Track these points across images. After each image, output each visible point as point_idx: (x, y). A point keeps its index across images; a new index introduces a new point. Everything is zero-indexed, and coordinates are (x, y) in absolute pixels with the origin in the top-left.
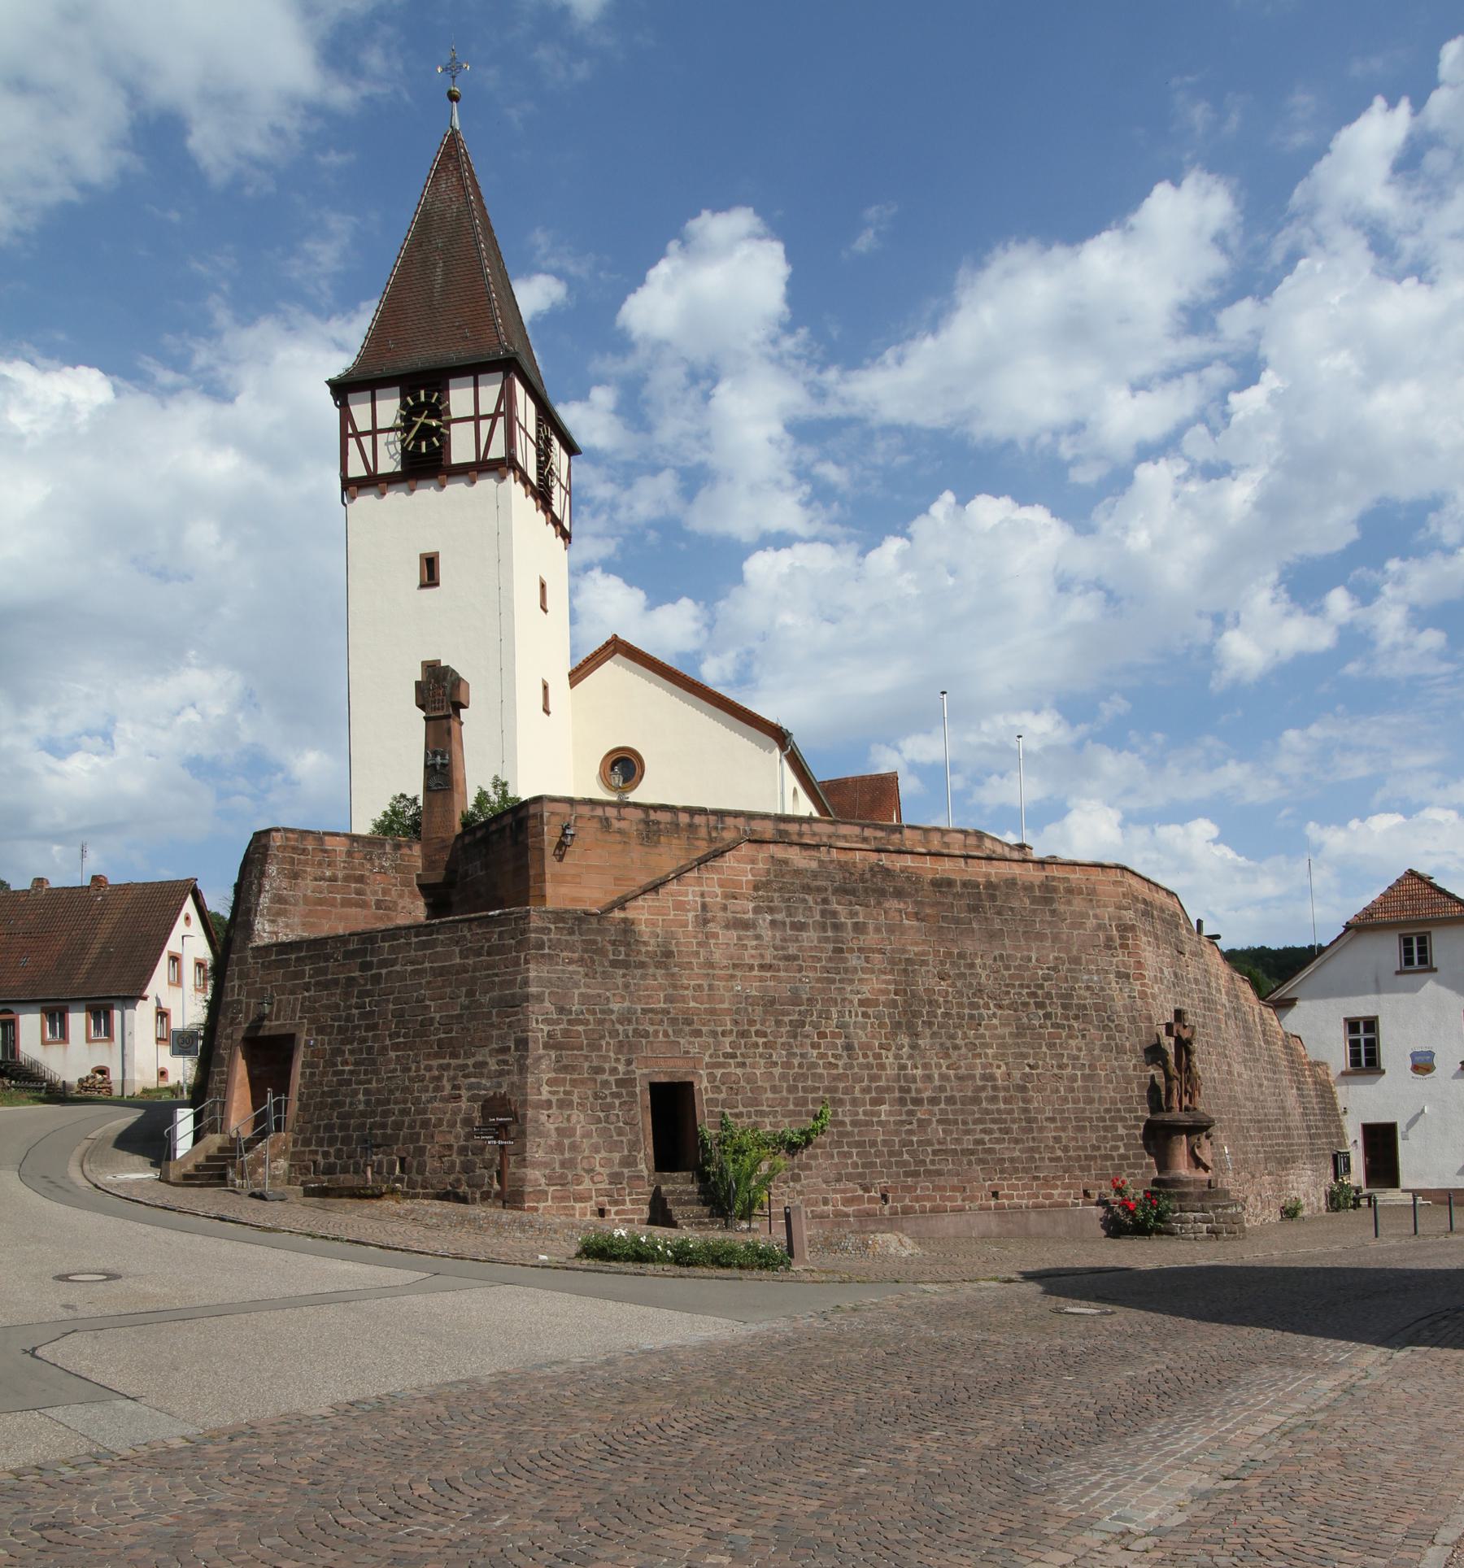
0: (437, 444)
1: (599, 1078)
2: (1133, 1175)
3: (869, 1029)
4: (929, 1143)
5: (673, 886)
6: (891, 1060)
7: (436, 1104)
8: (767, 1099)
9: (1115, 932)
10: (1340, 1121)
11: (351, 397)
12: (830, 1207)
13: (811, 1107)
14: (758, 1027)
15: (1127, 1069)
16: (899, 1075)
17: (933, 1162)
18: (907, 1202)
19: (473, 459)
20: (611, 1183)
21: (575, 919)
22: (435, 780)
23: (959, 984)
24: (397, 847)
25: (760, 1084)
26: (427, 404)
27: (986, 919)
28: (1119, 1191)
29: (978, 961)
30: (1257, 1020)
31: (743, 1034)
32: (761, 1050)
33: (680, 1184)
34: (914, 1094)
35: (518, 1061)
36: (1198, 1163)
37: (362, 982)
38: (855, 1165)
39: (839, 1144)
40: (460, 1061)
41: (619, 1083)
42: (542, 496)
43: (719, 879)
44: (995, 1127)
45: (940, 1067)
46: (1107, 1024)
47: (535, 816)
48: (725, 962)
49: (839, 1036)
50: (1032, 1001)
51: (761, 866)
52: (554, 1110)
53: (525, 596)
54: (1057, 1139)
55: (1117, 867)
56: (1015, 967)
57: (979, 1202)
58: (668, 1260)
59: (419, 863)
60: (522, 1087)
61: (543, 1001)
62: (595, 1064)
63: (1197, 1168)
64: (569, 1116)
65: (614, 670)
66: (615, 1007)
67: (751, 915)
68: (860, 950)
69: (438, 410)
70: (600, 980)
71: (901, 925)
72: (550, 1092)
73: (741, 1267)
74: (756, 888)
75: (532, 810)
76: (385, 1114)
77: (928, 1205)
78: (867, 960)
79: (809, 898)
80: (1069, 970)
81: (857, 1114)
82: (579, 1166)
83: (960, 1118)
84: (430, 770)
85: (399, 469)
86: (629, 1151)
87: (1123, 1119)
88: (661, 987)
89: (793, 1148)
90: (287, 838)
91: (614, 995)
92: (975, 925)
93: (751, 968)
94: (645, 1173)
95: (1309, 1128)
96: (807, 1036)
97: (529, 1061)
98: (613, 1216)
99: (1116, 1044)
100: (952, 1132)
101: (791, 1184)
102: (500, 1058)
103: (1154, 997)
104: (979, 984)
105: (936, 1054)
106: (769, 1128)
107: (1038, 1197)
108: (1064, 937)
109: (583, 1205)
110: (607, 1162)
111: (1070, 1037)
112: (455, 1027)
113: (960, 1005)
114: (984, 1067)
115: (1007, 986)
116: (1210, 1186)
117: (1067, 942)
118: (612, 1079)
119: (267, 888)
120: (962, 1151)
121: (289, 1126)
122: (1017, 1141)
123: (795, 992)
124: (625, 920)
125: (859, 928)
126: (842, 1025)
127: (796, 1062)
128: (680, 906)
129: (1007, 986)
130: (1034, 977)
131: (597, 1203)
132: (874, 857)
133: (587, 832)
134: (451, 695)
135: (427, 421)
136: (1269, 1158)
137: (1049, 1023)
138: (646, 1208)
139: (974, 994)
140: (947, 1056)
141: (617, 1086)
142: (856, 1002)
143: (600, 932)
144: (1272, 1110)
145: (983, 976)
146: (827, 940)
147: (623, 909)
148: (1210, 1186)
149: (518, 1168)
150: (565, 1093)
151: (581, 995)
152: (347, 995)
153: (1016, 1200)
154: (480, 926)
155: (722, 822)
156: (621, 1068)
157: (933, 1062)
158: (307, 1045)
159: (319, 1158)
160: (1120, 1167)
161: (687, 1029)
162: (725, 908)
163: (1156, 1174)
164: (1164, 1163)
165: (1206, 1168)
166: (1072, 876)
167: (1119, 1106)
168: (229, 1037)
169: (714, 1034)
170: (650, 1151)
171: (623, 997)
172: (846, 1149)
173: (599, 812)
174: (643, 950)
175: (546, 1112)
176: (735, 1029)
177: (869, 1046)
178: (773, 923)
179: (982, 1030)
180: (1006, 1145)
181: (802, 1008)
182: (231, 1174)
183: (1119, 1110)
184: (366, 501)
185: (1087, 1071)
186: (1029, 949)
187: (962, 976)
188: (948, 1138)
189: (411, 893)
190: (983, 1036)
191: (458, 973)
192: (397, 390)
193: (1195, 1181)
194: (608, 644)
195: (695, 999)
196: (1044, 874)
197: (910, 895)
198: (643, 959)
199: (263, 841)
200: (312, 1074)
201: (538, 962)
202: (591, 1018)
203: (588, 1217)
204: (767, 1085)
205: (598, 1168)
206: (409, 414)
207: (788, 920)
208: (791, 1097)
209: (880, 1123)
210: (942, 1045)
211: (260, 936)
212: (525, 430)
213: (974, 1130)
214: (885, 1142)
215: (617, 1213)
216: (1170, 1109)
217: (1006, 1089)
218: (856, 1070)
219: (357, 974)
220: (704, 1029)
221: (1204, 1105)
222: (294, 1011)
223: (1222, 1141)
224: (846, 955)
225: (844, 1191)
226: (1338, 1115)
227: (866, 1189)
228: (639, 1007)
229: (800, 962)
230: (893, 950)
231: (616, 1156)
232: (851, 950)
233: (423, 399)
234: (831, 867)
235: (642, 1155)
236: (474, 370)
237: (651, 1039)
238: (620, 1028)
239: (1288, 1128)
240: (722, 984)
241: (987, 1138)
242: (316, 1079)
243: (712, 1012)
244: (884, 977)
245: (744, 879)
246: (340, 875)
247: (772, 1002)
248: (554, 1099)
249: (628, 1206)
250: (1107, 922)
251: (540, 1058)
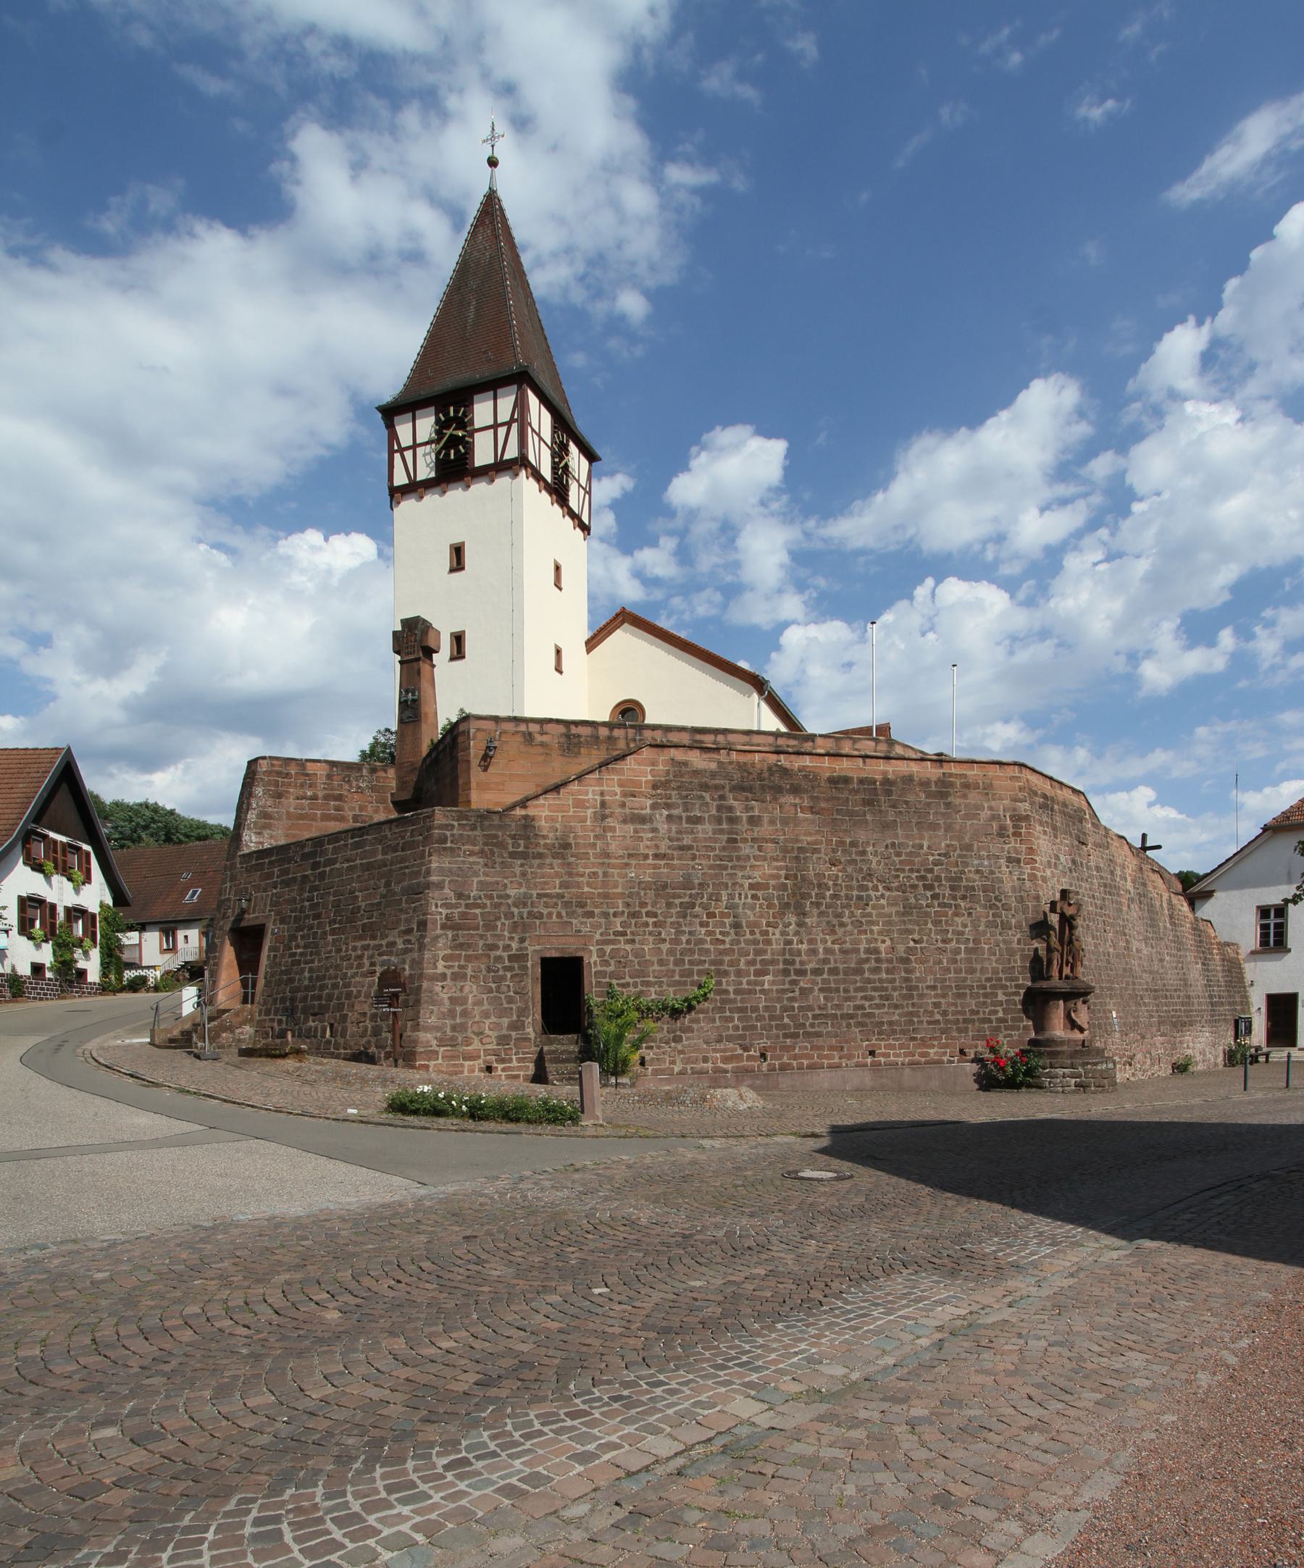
0: (463, 451)
1: (493, 954)
2: (1011, 1036)
3: (758, 910)
4: (810, 1008)
5: (574, 787)
6: (778, 936)
7: (357, 979)
8: (654, 971)
9: (1008, 822)
10: (1246, 992)
11: (397, 419)
12: (710, 1065)
13: (696, 978)
14: (649, 908)
15: (1011, 943)
16: (784, 949)
17: (812, 1025)
18: (785, 1059)
19: (492, 461)
20: (498, 1044)
21: (478, 816)
22: (408, 713)
23: (849, 869)
24: (373, 770)
25: (647, 958)
26: (456, 418)
27: (880, 811)
28: (993, 1050)
29: (870, 849)
30: (1165, 905)
31: (634, 915)
32: (651, 928)
33: (567, 1044)
34: (798, 966)
35: (418, 940)
36: (1073, 1025)
37: (312, 878)
38: (737, 1028)
39: (721, 1010)
40: (376, 942)
41: (511, 958)
42: (558, 491)
43: (619, 780)
44: (876, 994)
45: (824, 941)
46: (994, 899)
47: (463, 732)
48: (621, 852)
49: (728, 915)
50: (921, 883)
51: (661, 767)
52: (448, 982)
53: (536, 575)
54: (937, 1005)
55: (1015, 764)
56: (906, 853)
57: (856, 1060)
58: (463, 1115)
59: (394, 784)
60: (417, 964)
61: (442, 888)
62: (490, 942)
63: (1072, 1029)
64: (462, 987)
65: (623, 638)
66: (512, 892)
67: (648, 811)
68: (753, 840)
69: (464, 422)
70: (498, 869)
71: (796, 817)
72: (445, 967)
73: (529, 1121)
74: (655, 787)
75: (462, 727)
76: (322, 988)
77: (805, 1062)
78: (760, 849)
79: (707, 796)
80: (960, 856)
81: (741, 983)
82: (470, 1030)
83: (842, 987)
84: (403, 705)
85: (433, 475)
86: (518, 1017)
87: (1004, 987)
88: (557, 875)
89: (676, 1013)
90: (273, 765)
91: (511, 882)
92: (868, 817)
93: (646, 857)
94: (532, 1036)
95: (1211, 997)
96: (696, 916)
97: (427, 940)
98: (499, 1072)
99: (1002, 921)
100: (833, 999)
101: (673, 1044)
102: (406, 938)
103: (1044, 879)
104: (869, 869)
105: (822, 931)
106: (654, 996)
107: (914, 1055)
108: (958, 827)
109: (471, 1063)
110: (497, 1026)
111: (956, 914)
112: (375, 913)
113: (850, 888)
114: (869, 941)
115: (897, 870)
116: (1083, 1046)
117: (960, 831)
118: (505, 955)
119: (254, 806)
120: (842, 1016)
121: (257, 999)
122: (896, 1007)
123: (688, 878)
124: (526, 817)
125: (753, 821)
126: (730, 906)
127: (684, 939)
128: (580, 804)
129: (897, 870)
130: (925, 862)
131: (485, 1061)
132: (773, 758)
133: (511, 747)
134: (421, 641)
135: (455, 433)
136: (1164, 1022)
137: (936, 903)
138: (531, 1065)
139: (864, 878)
140: (833, 932)
141: (509, 961)
142: (746, 886)
143: (500, 827)
144: (1172, 979)
145: (874, 863)
146: (721, 831)
147: (525, 807)
148: (1083, 1046)
149: (412, 1031)
150: (460, 967)
151: (480, 882)
152: (302, 890)
153: (892, 1058)
154: (397, 826)
155: (641, 735)
156: (514, 945)
157: (819, 938)
158: (273, 934)
159: (276, 1025)
160: (998, 1029)
161: (580, 911)
162: (623, 805)
163: (1033, 1035)
164: (1040, 1026)
165: (1082, 1030)
166: (969, 773)
167: (1001, 975)
168: (221, 929)
169: (606, 915)
170: (538, 1017)
171: (520, 885)
172: (728, 1014)
173: (523, 728)
174: (542, 842)
175: (440, 984)
176: (626, 911)
177: (757, 924)
178: (669, 818)
179: (869, 910)
180: (886, 1010)
181: (693, 892)
182: (195, 1039)
183: (1000, 979)
184: (407, 506)
185: (971, 945)
186: (922, 838)
187: (853, 862)
188: (829, 1005)
189: (385, 808)
190: (870, 915)
191: (380, 867)
192: (432, 409)
193: (1069, 1041)
194: (617, 615)
195: (589, 885)
196: (942, 771)
197: (806, 791)
198: (541, 850)
199: (253, 768)
200: (275, 956)
201: (440, 854)
202: (488, 902)
203: (476, 1073)
204: (655, 959)
205: (487, 1032)
206: (441, 426)
207: (684, 815)
208: (677, 969)
209: (762, 991)
210: (828, 923)
211: (247, 846)
212: (538, 435)
213: (855, 998)
214: (766, 1009)
215: (503, 1070)
216: (1049, 978)
217: (889, 961)
218: (743, 945)
219: (309, 872)
220: (597, 911)
221: (1085, 974)
222: (265, 905)
223: (1111, 1007)
224: (740, 845)
225: (724, 1051)
226: (1245, 987)
227: (746, 1049)
228: (534, 893)
229: (695, 852)
230: (786, 840)
231: (505, 1021)
232: (745, 840)
233: (452, 414)
234: (730, 767)
235: (530, 1020)
236: (492, 386)
237: (545, 920)
238: (515, 910)
239: (1188, 997)
240: (616, 871)
241: (867, 1004)
242: (278, 960)
243: (606, 896)
244: (776, 864)
245: (644, 779)
246: (320, 794)
247: (665, 886)
248: (449, 972)
249: (515, 1064)
250: (1001, 813)
251: (438, 937)
